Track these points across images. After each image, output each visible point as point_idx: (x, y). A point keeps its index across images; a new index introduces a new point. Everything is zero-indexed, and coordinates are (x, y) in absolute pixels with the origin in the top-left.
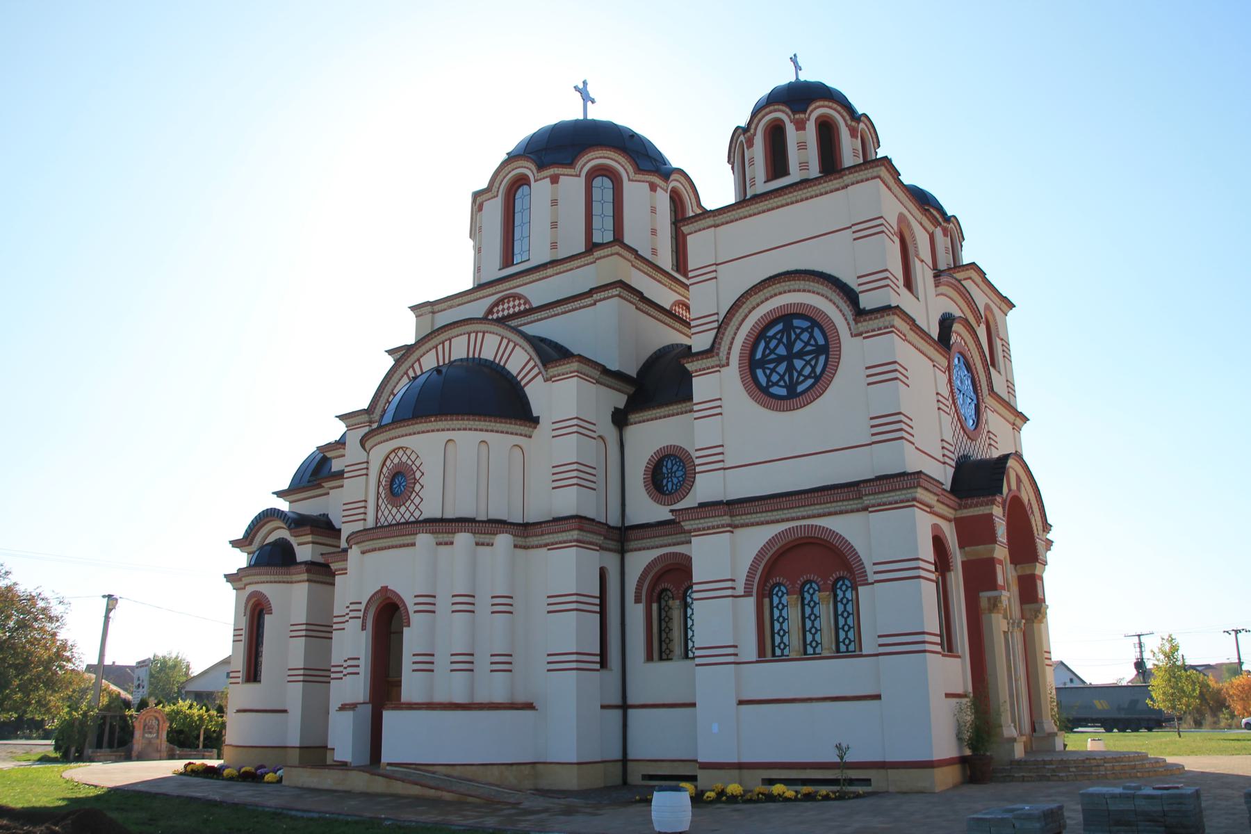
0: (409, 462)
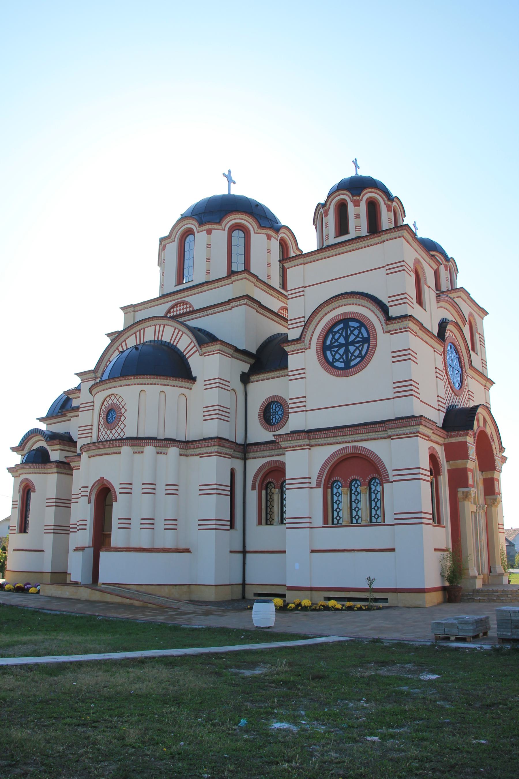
0: (118, 403)
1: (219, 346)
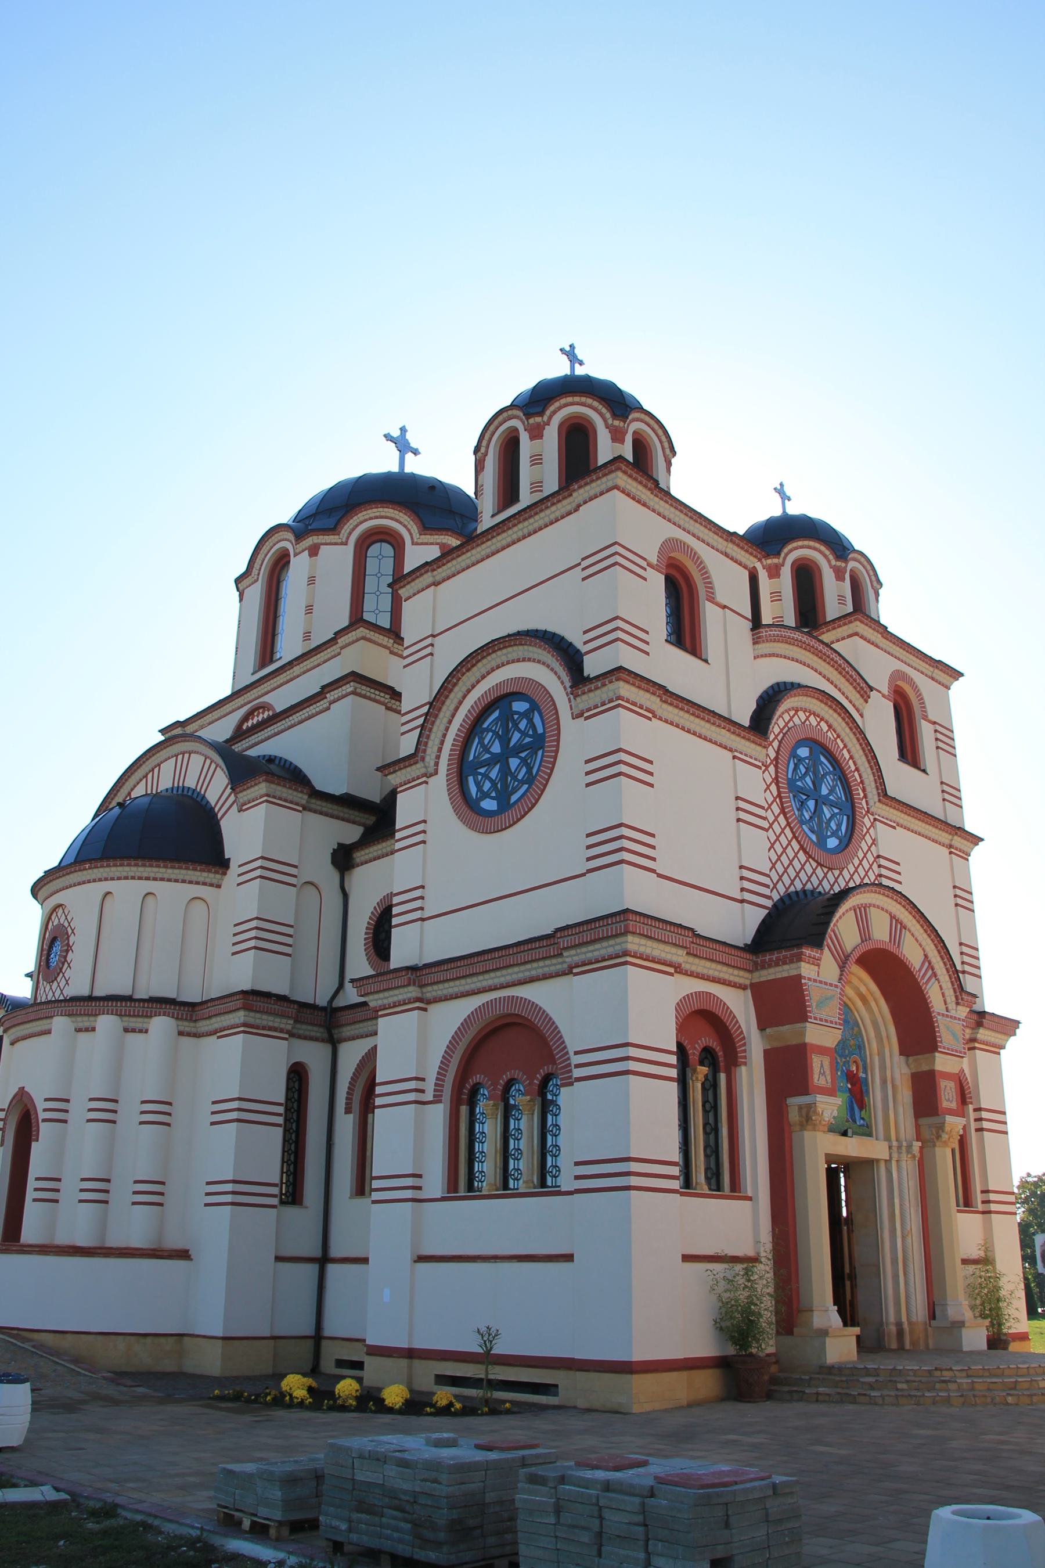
1: (263, 785)
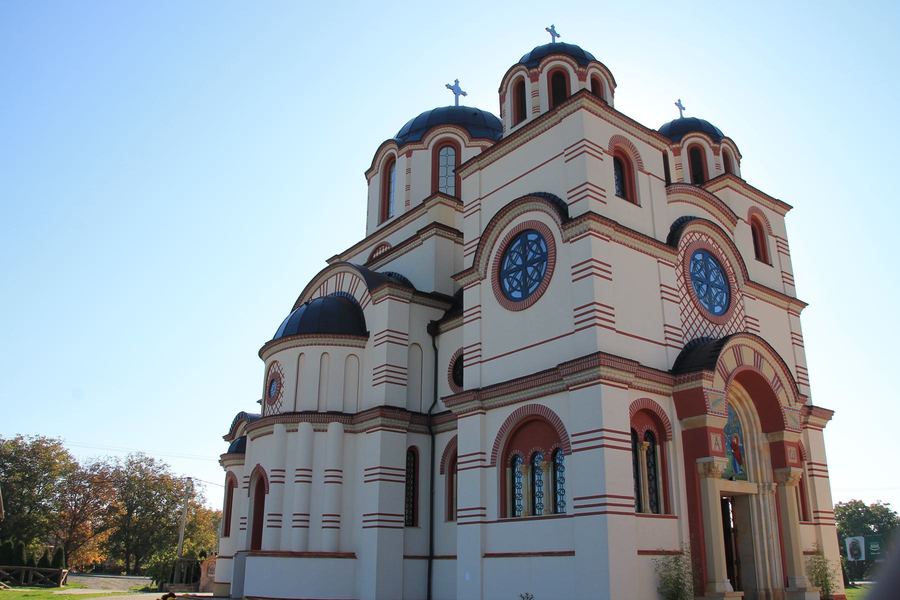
1: (387, 289)
